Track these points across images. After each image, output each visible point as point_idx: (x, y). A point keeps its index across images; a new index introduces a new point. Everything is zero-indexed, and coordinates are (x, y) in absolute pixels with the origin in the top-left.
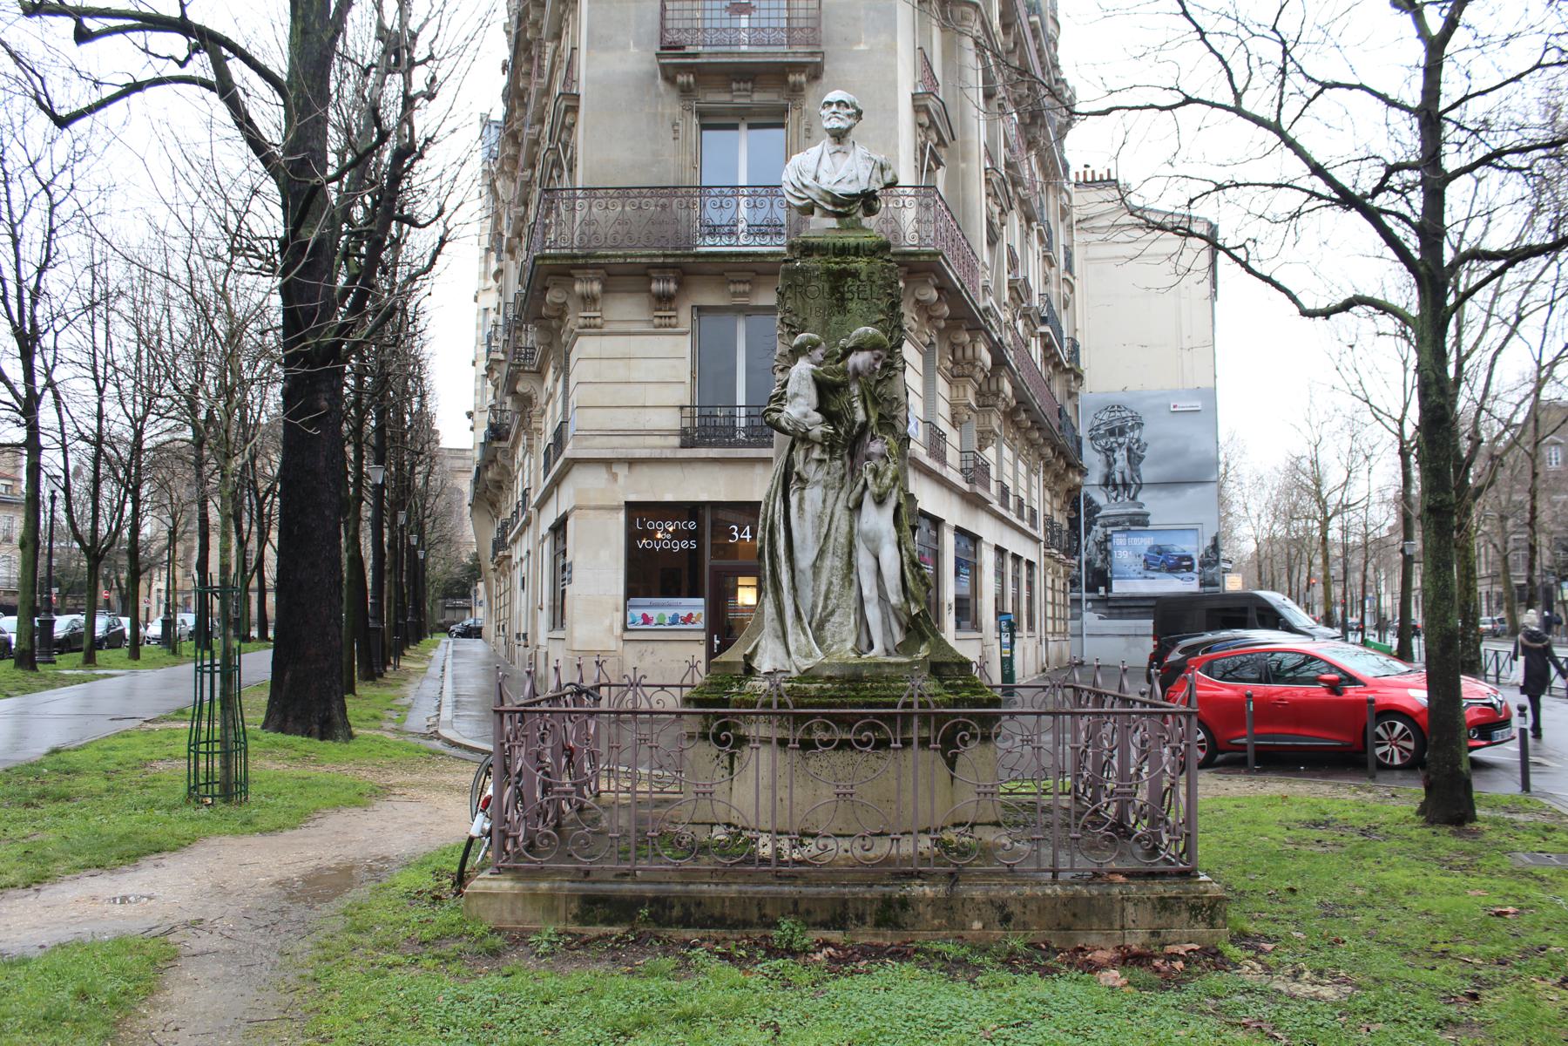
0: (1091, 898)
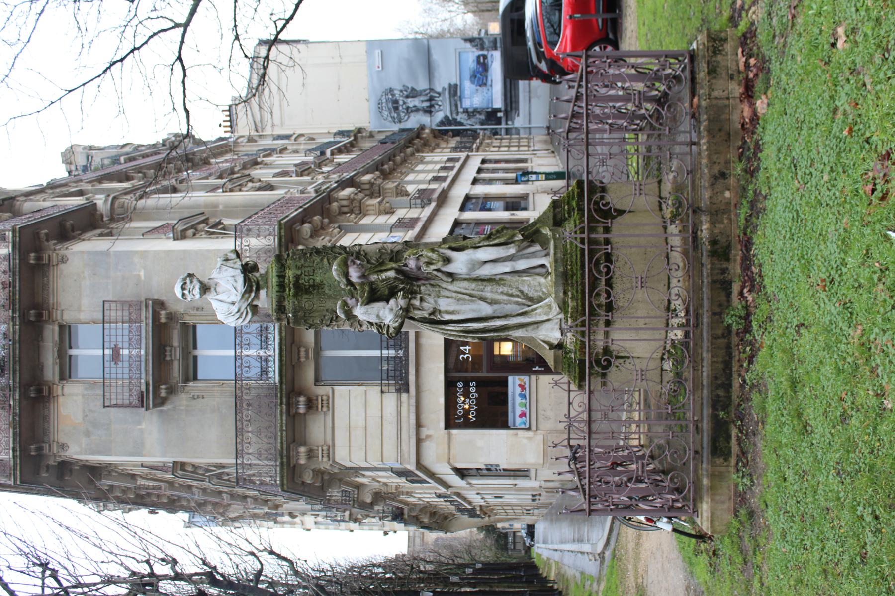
0: (709, 119)
